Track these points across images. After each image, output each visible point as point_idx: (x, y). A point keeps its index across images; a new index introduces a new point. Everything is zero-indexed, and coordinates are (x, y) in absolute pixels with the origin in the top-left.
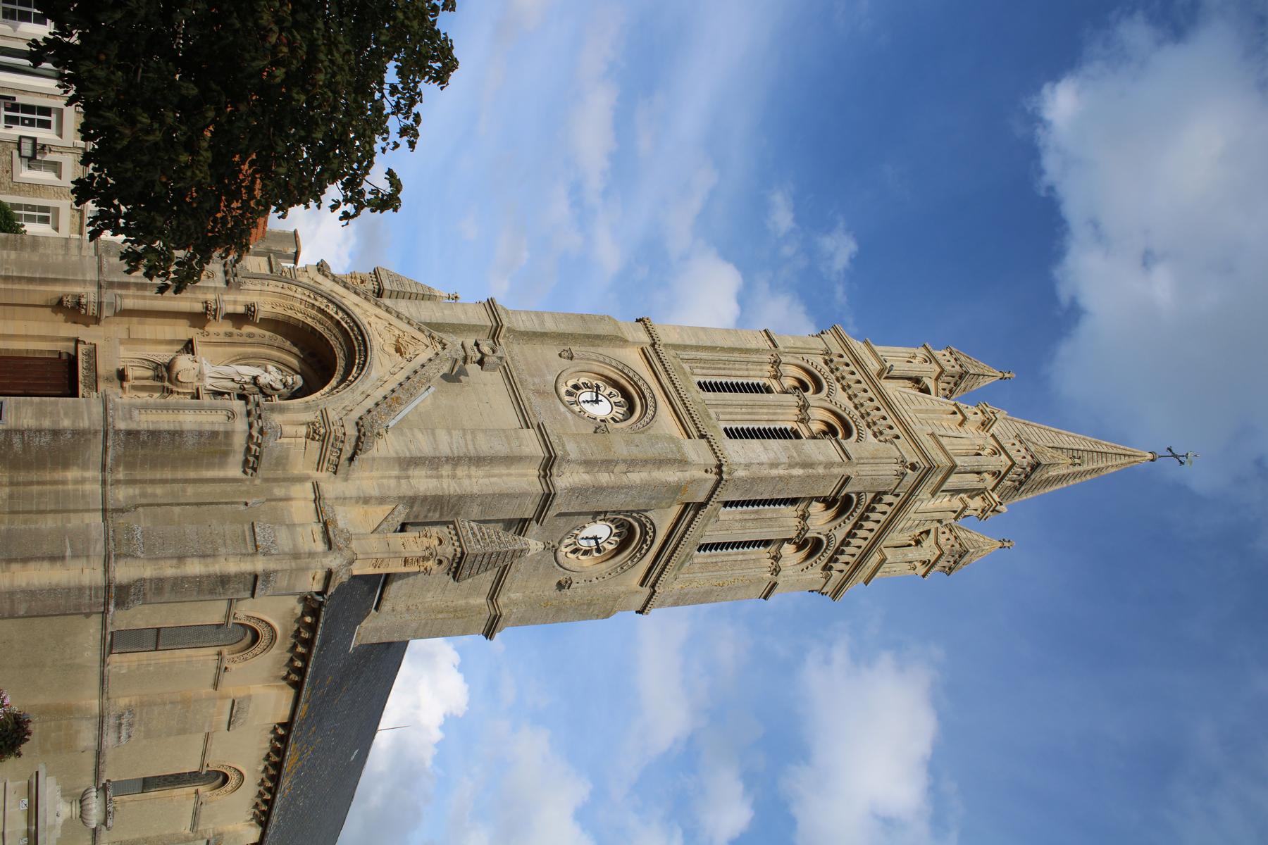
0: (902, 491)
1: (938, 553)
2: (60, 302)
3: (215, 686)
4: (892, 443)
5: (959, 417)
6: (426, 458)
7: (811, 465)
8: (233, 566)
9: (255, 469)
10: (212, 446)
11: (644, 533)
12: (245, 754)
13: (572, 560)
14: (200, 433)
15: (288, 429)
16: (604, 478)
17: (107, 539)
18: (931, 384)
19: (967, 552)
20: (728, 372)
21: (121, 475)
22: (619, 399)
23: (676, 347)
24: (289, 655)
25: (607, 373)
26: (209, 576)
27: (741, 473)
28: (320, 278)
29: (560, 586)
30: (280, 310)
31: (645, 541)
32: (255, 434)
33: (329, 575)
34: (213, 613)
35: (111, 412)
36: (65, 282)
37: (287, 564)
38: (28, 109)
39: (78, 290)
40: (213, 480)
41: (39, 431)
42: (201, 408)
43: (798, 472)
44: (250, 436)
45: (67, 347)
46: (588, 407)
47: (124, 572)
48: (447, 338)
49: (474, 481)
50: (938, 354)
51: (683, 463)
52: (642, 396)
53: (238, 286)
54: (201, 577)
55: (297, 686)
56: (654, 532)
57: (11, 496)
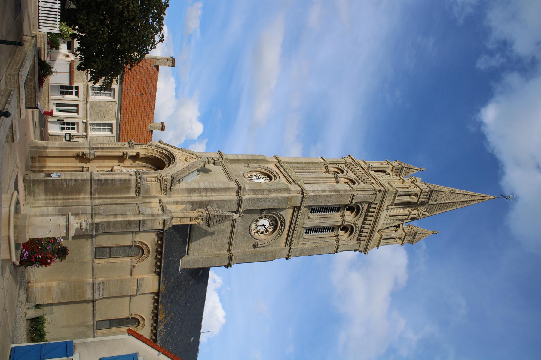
1: (404, 233)
2: (78, 154)
3: (131, 275)
5: (401, 180)
6: (196, 189)
9: (139, 193)
11: (281, 222)
13: (257, 236)
16: (260, 196)
18: (390, 172)
21: (97, 196)
22: (267, 178)
23: (287, 163)
24: (155, 261)
25: (262, 171)
26: (124, 221)
28: (160, 144)
29: (255, 246)
31: (282, 225)
32: (138, 179)
34: (126, 240)
36: (79, 148)
38: (68, 124)
39: (83, 150)
41: (71, 180)
44: (137, 180)
46: (256, 181)
51: (288, 190)
54: (122, 221)
55: (159, 274)
57: (63, 203)
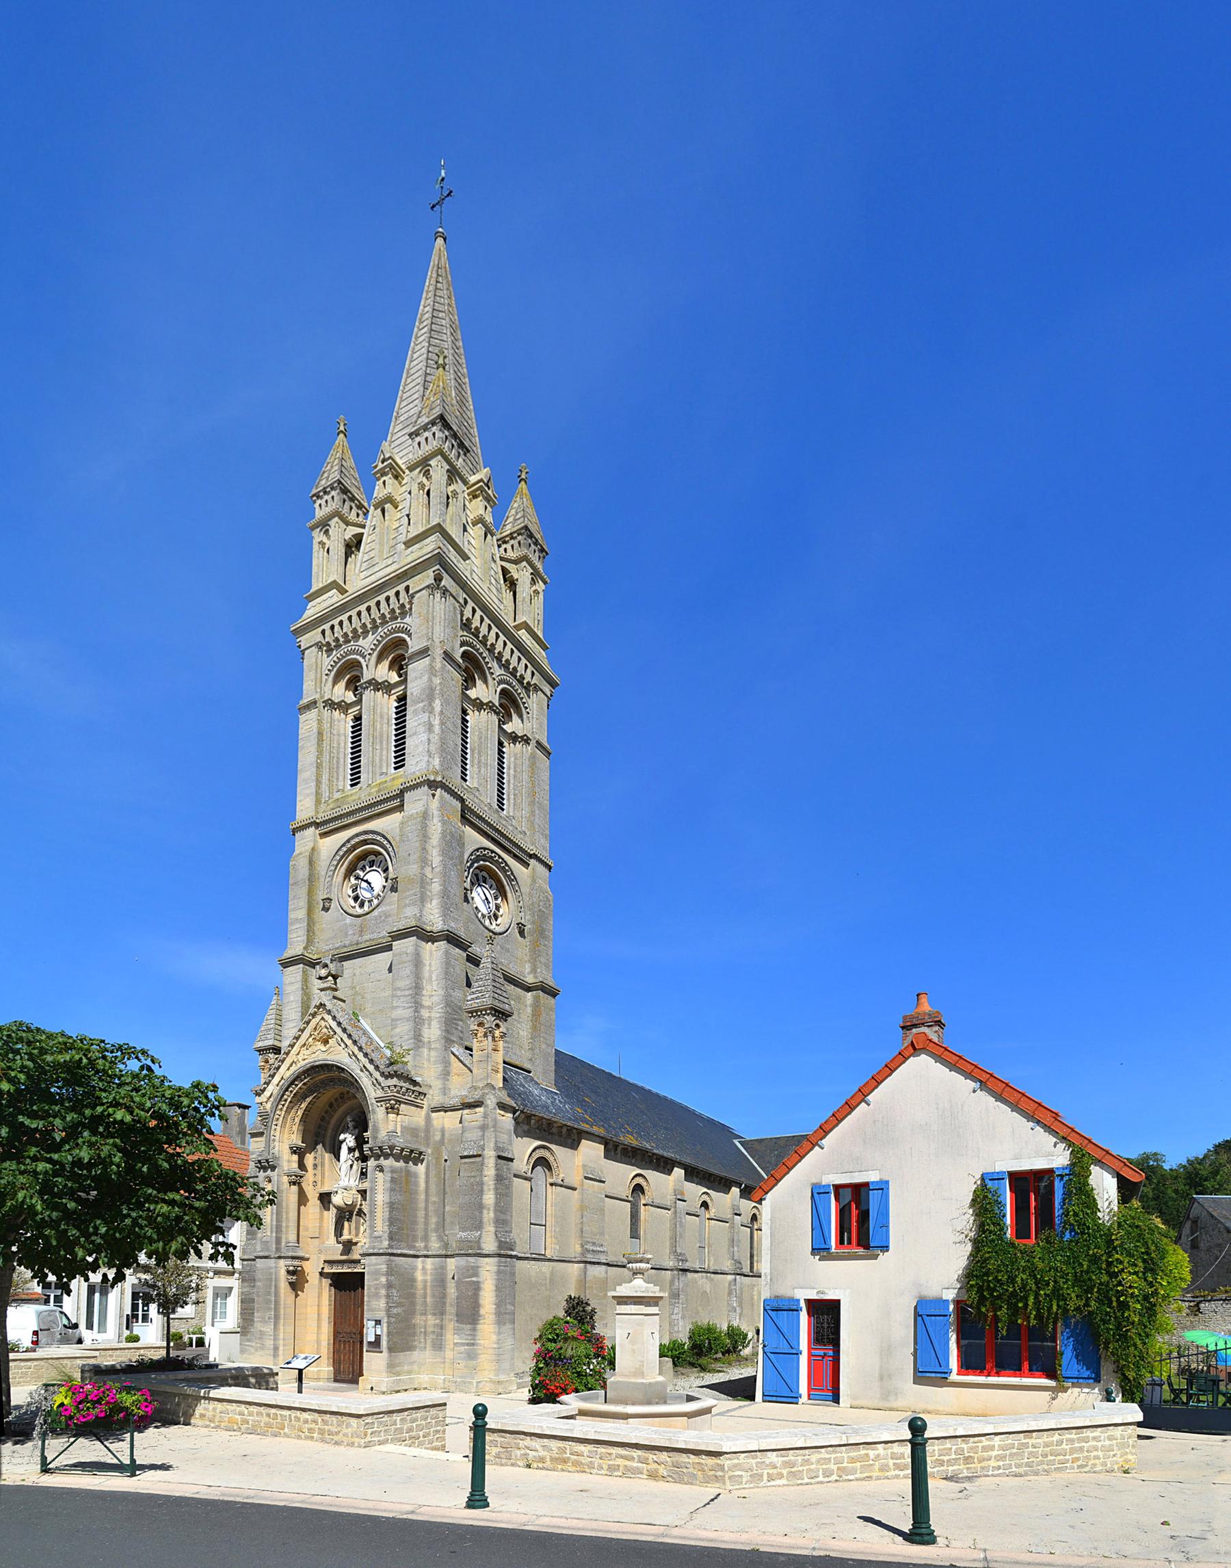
0: (462, 596)
1: (524, 563)
3: (574, 1189)
4: (412, 596)
7: (432, 689)
8: (490, 1171)
9: (421, 1153)
10: (402, 1184)
11: (485, 858)
12: (622, 1174)
14: (392, 1190)
15: (391, 1128)
16: (436, 887)
17: (467, 1255)
18: (352, 531)
19: (526, 527)
20: (341, 756)
23: (318, 802)
27: (436, 762)
28: (267, 1093)
29: (522, 933)
30: (295, 1128)
33: (502, 1106)
35: (376, 1251)
37: (490, 1134)
40: (427, 1182)
41: (388, 1296)
42: (373, 1189)
43: (437, 704)
45: (326, 1282)
47: (489, 1245)
48: (316, 1002)
49: (433, 993)
50: (319, 514)
51: (425, 815)
52: (365, 842)
53: (275, 1158)
54: (496, 1194)
56: (485, 849)
